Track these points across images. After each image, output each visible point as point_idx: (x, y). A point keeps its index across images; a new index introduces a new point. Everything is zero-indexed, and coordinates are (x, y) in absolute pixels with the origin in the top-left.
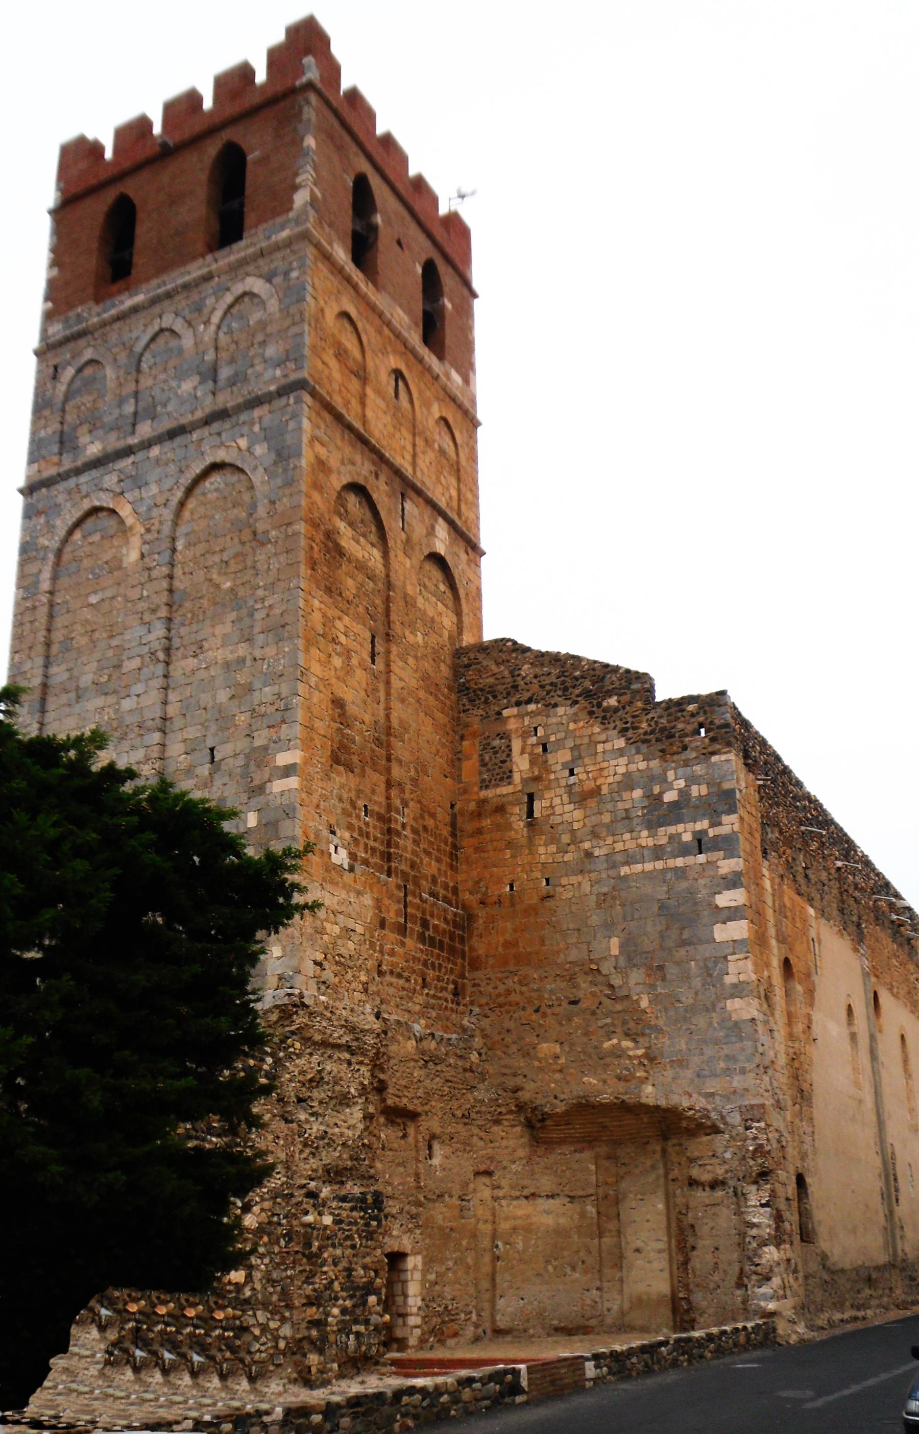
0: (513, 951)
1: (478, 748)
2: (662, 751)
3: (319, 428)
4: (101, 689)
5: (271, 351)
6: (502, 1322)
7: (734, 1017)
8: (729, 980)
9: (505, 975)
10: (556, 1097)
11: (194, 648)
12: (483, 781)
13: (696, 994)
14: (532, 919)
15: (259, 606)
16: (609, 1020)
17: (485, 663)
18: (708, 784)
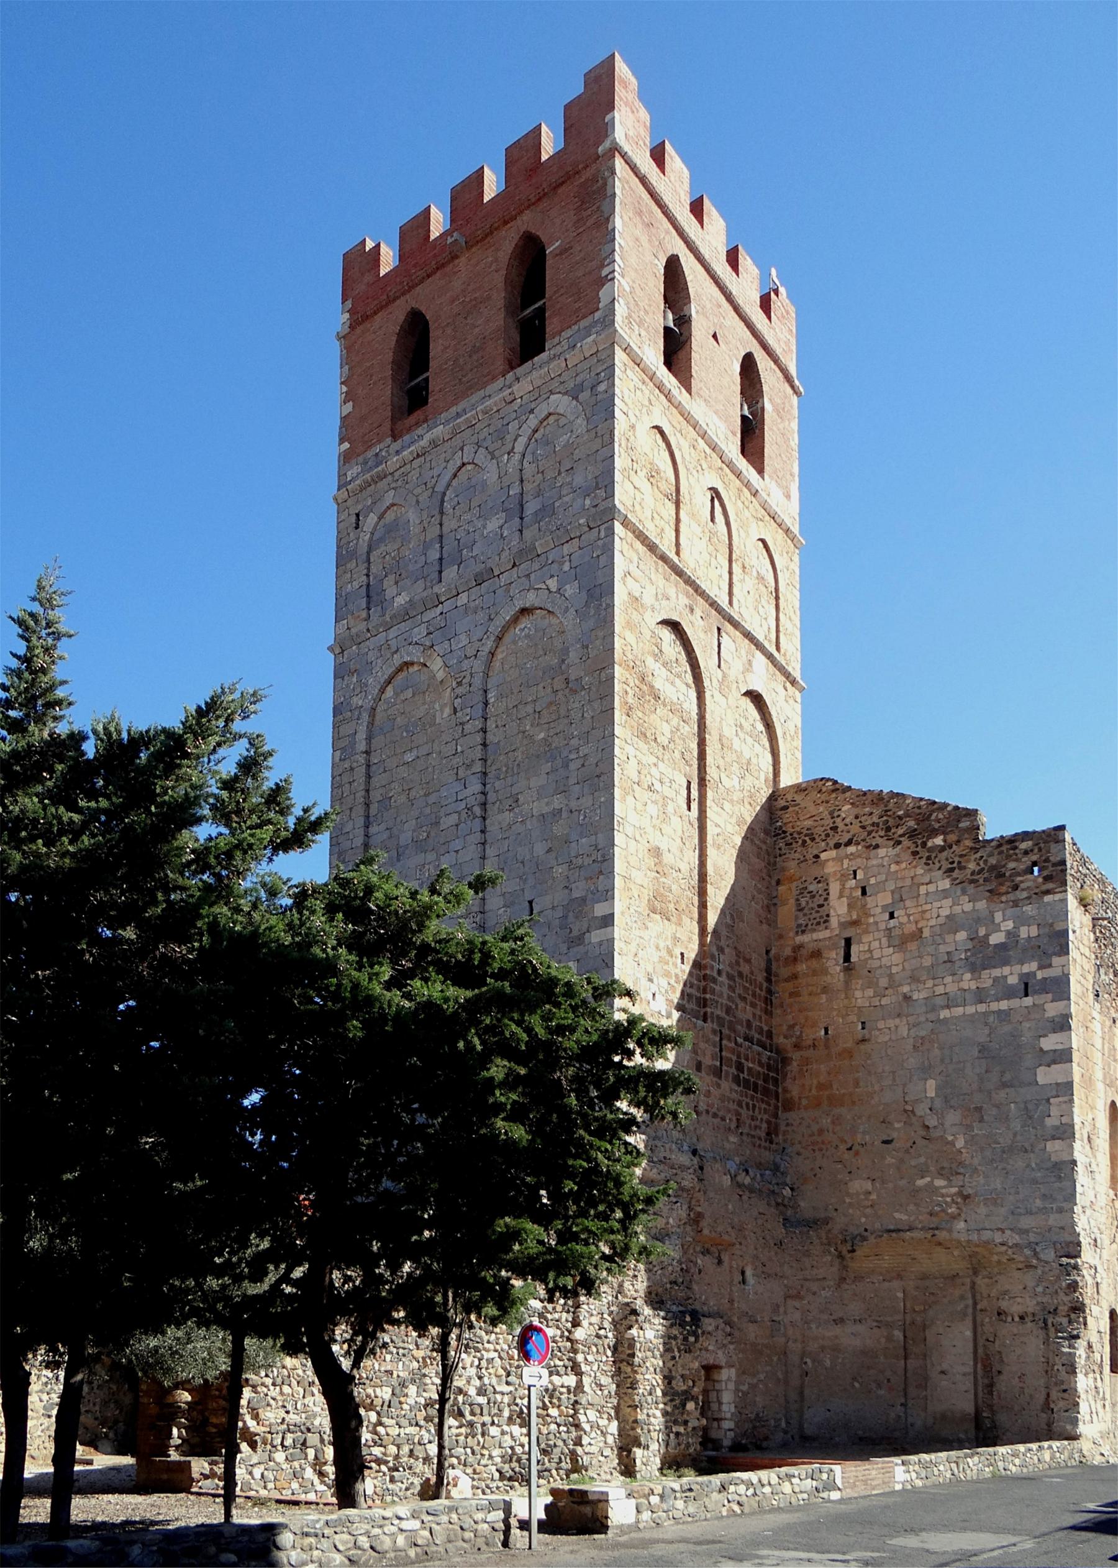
4: (420, 846)
12: (799, 926)
15: (572, 756)
18: (1039, 925)
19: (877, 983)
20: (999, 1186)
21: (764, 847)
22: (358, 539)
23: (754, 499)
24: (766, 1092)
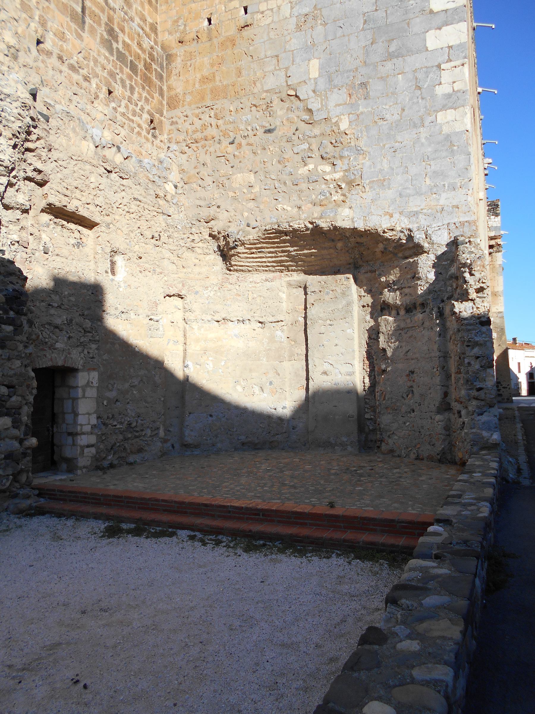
0: (209, 86)
6: (190, 437)
7: (446, 130)
8: (440, 91)
14: (229, 51)
16: (305, 146)
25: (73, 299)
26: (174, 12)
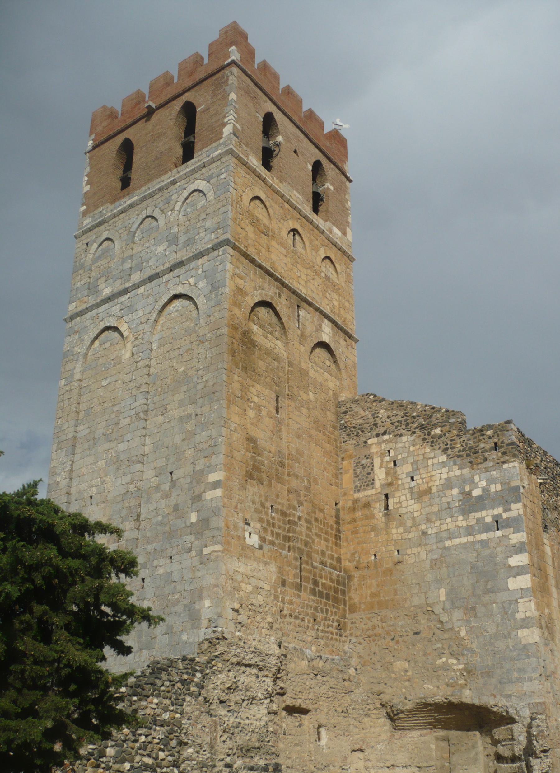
1: (353, 465)
2: (471, 462)
3: (238, 268)
4: (108, 438)
5: (209, 224)
7: (524, 642)
8: (520, 616)
9: (371, 615)
10: (406, 698)
11: (162, 409)
12: (356, 487)
13: (498, 626)
14: (389, 578)
15: (199, 381)
16: (440, 645)
17: (356, 410)
18: (501, 483)
19: (405, 524)
20: (490, 663)
21: (332, 436)
22: (86, 257)
23: (322, 236)
24: (336, 600)
25: (297, 761)
26: (352, 548)
